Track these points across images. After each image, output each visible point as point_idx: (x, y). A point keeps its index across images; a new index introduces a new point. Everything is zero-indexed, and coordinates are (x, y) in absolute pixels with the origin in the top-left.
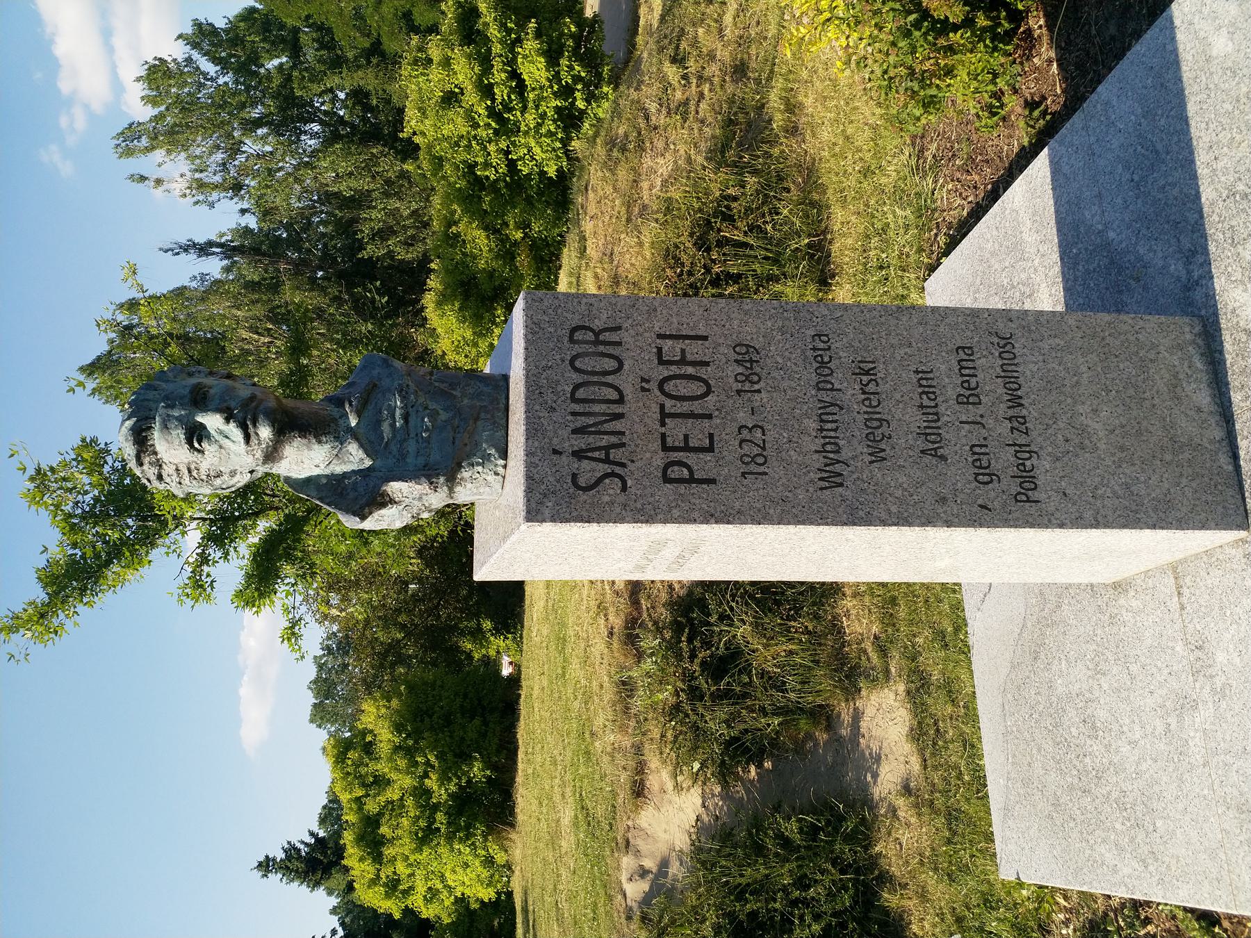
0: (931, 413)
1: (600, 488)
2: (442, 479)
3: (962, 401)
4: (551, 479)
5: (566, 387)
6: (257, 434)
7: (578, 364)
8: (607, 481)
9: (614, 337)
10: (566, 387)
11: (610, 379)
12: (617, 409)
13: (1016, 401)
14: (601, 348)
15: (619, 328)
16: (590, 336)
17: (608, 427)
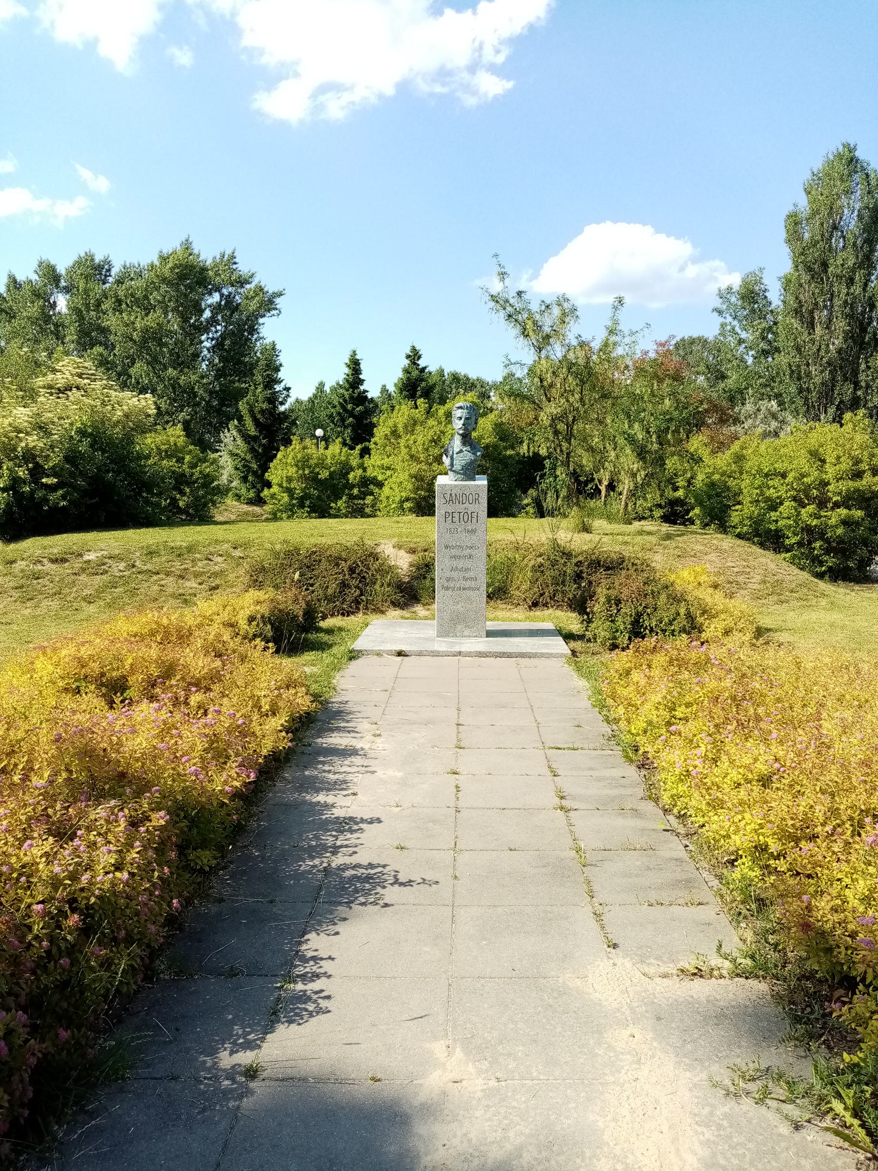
0: (461, 570)
2: (519, 493)
3: (464, 577)
13: (464, 589)
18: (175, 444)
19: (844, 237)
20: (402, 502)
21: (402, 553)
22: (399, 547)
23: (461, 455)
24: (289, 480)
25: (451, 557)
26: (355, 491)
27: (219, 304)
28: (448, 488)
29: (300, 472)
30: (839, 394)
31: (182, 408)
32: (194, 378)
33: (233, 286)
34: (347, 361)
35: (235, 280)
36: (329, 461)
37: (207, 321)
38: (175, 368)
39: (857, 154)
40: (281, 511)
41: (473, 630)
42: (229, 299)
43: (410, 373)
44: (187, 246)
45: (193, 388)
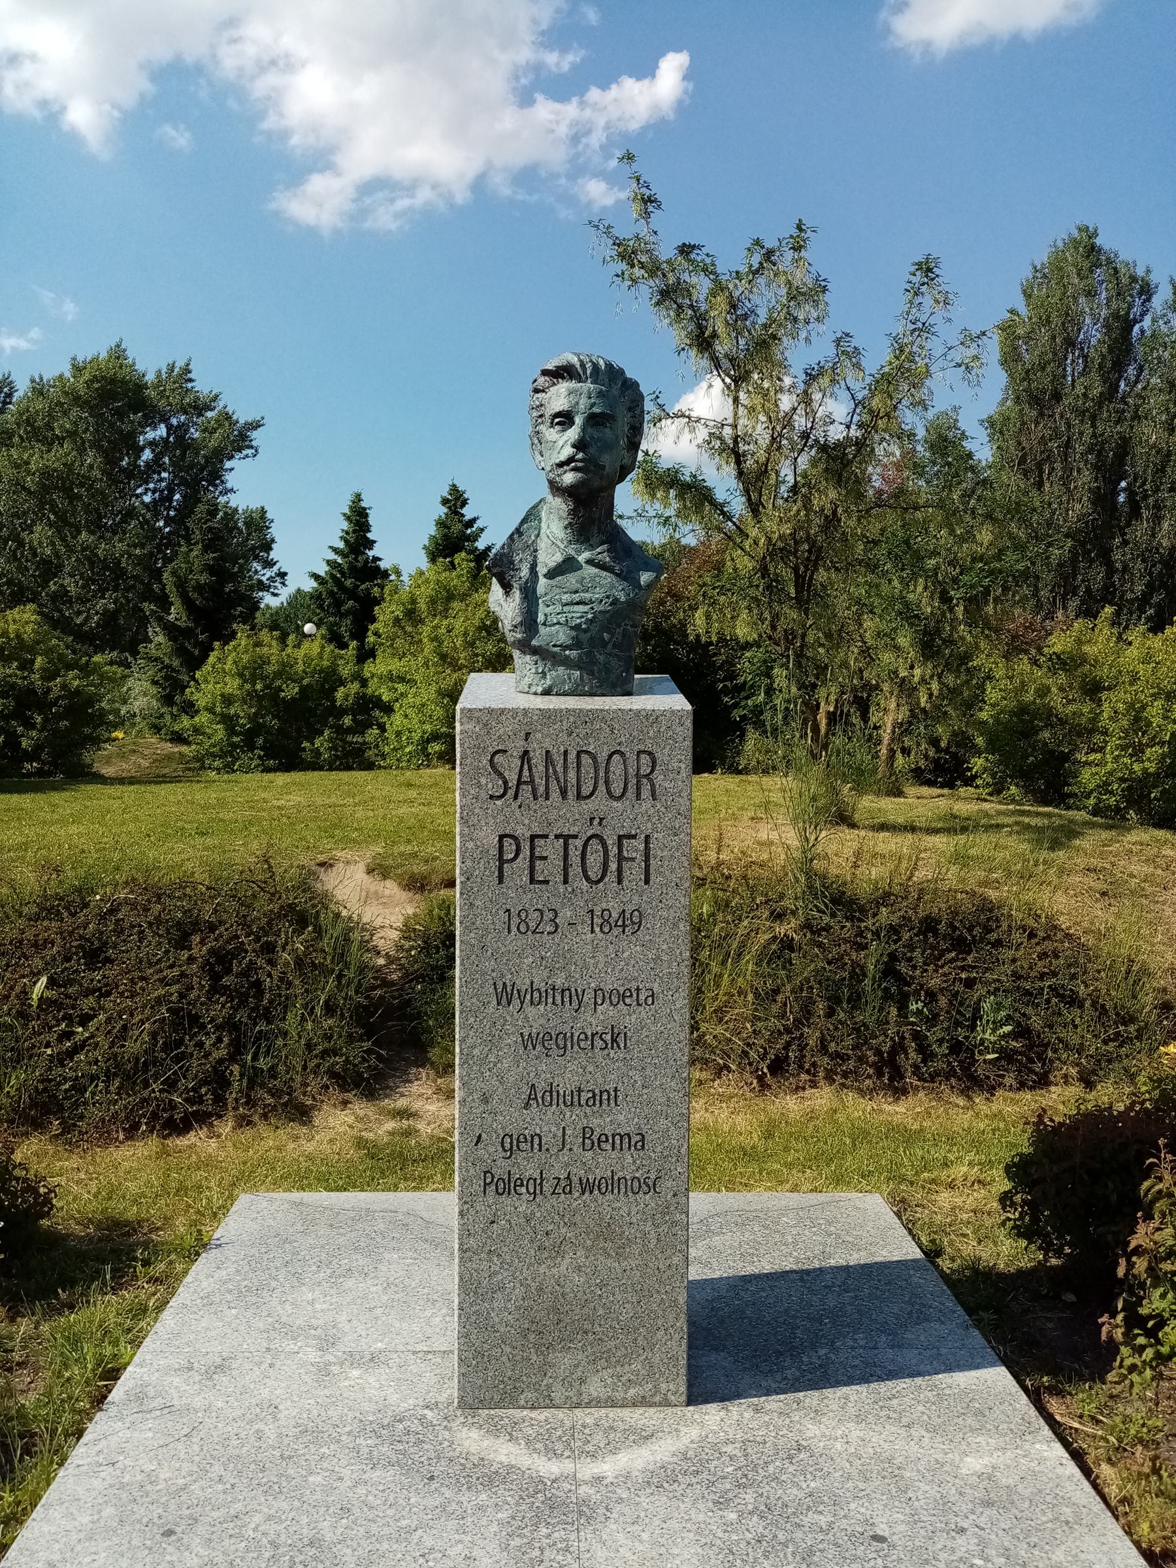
0: (573, 1099)
7: (616, 757)
8: (500, 782)
11: (602, 788)
12: (572, 793)
13: (587, 1187)
17: (554, 786)
18: (18, 636)
19: (1085, 357)
20: (426, 741)
21: (391, 888)
22: (380, 870)
23: (571, 580)
24: (228, 700)
25: (529, 1042)
26: (347, 721)
27: (166, 441)
28: (508, 727)
29: (248, 686)
30: (1083, 581)
31: (102, 591)
33: (186, 413)
34: (347, 511)
35: (189, 405)
36: (300, 667)
38: (92, 533)
39: (1098, 241)
40: (214, 755)
41: (627, 1372)
42: (179, 432)
43: (449, 528)
44: (118, 353)
45: (119, 562)
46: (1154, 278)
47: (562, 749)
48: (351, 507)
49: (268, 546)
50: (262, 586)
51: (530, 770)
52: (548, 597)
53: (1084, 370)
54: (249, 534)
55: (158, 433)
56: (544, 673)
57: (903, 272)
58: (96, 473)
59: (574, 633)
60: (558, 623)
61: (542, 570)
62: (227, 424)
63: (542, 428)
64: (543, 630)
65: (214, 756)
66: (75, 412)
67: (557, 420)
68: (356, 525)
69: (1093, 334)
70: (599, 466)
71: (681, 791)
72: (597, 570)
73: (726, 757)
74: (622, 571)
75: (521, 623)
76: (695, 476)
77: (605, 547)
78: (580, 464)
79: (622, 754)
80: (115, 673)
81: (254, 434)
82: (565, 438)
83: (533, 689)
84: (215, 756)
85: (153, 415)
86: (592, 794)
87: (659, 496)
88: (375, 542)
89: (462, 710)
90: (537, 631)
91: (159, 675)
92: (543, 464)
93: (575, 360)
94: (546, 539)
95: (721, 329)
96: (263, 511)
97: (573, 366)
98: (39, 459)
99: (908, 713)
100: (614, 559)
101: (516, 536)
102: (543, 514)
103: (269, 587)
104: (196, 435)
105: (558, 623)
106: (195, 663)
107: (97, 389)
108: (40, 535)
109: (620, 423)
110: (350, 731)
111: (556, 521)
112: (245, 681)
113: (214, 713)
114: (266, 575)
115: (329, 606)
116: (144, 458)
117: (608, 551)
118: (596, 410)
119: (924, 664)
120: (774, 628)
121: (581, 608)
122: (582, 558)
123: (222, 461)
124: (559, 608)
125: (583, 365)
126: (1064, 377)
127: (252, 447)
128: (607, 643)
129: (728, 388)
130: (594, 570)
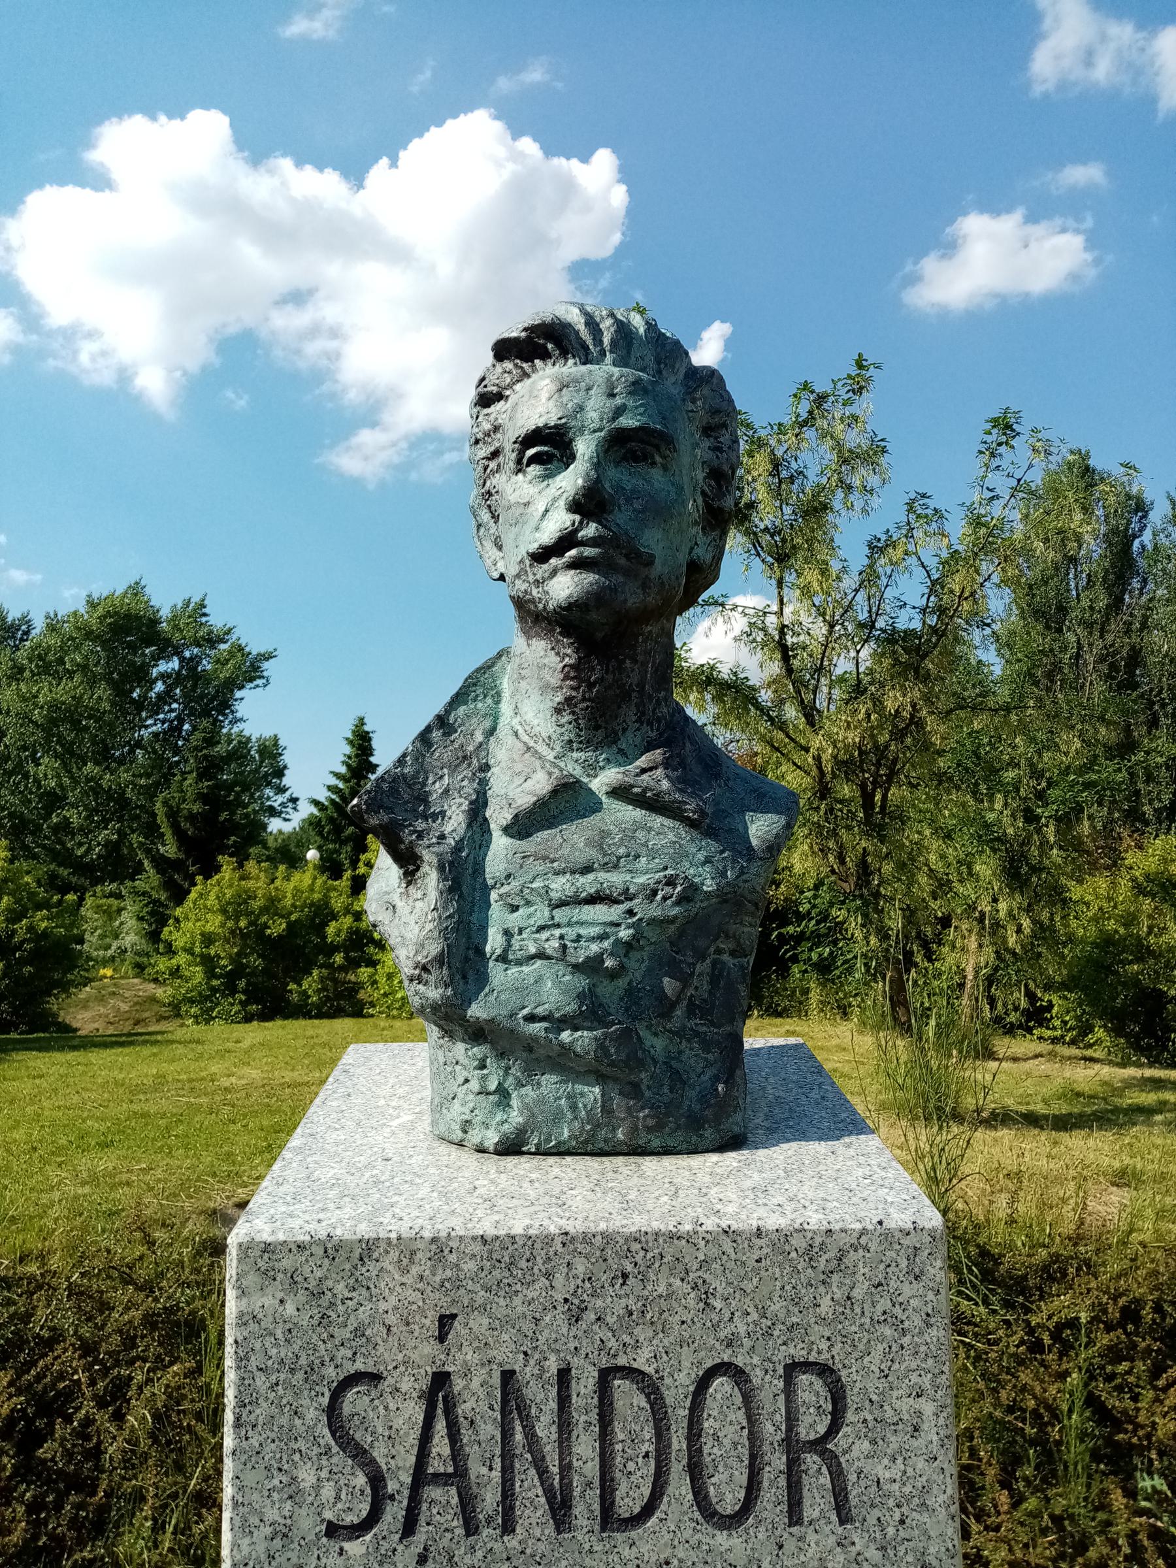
1: (339, 1458)
4: (364, 1314)
5: (646, 1353)
6: (554, 573)
7: (721, 1386)
8: (361, 1480)
9: (817, 1502)
10: (646, 1353)
11: (679, 1486)
12: (585, 1509)
14: (779, 1461)
15: (844, 1518)
16: (812, 1425)
17: (529, 1486)
24: (208, 939)
26: (339, 959)
27: (179, 673)
29: (230, 924)
31: (105, 822)
32: (125, 776)
33: (199, 646)
34: (350, 736)
35: (203, 637)
36: (288, 902)
37: (159, 695)
38: (97, 763)
39: (1092, 463)
42: (191, 664)
44: (136, 590)
45: (124, 792)
46: (1148, 496)
47: (553, 1365)
48: (353, 732)
49: (280, 773)
50: (273, 812)
51: (454, 1435)
52: (515, 884)
53: (1088, 584)
54: (262, 762)
55: (170, 665)
56: (503, 1093)
57: (975, 432)
58: (105, 705)
59: (582, 982)
60: (541, 955)
61: (498, 816)
62: (239, 655)
63: (498, 481)
64: (498, 975)
65: (192, 1001)
66: (88, 645)
67: (531, 452)
68: (358, 749)
69: (1093, 548)
70: (639, 554)
71: (925, 1490)
72: (638, 813)
73: (763, 997)
74: (702, 813)
75: (440, 960)
76: (735, 674)
77: (657, 754)
78: (589, 552)
79: (737, 1374)
80: (110, 906)
81: (265, 665)
82: (552, 491)
83: (475, 1137)
84: (193, 1002)
85: (166, 648)
86: (648, 1510)
87: (691, 698)
88: (377, 766)
89: (245, 1249)
90: (482, 979)
91: (145, 910)
92: (501, 567)
93: (575, 317)
94: (510, 740)
95: (762, 494)
96: (276, 739)
97: (568, 326)
98: (48, 692)
99: (993, 955)
100: (683, 782)
101: (436, 735)
102: (506, 685)
103: (281, 812)
104: (209, 667)
105: (541, 955)
106: (179, 896)
107: (110, 624)
108: (47, 770)
109: (686, 460)
110: (342, 968)
111: (535, 696)
112: (229, 918)
113: (193, 954)
114: (277, 801)
115: (329, 833)
116: (156, 690)
117: (666, 764)
118: (628, 421)
119: (1011, 895)
120: (842, 861)
121: (601, 913)
122: (599, 783)
123: (232, 691)
124: (542, 913)
125: (592, 323)
126: (1069, 591)
127: (263, 677)
128: (673, 1005)
129: (771, 567)
130: (629, 813)
